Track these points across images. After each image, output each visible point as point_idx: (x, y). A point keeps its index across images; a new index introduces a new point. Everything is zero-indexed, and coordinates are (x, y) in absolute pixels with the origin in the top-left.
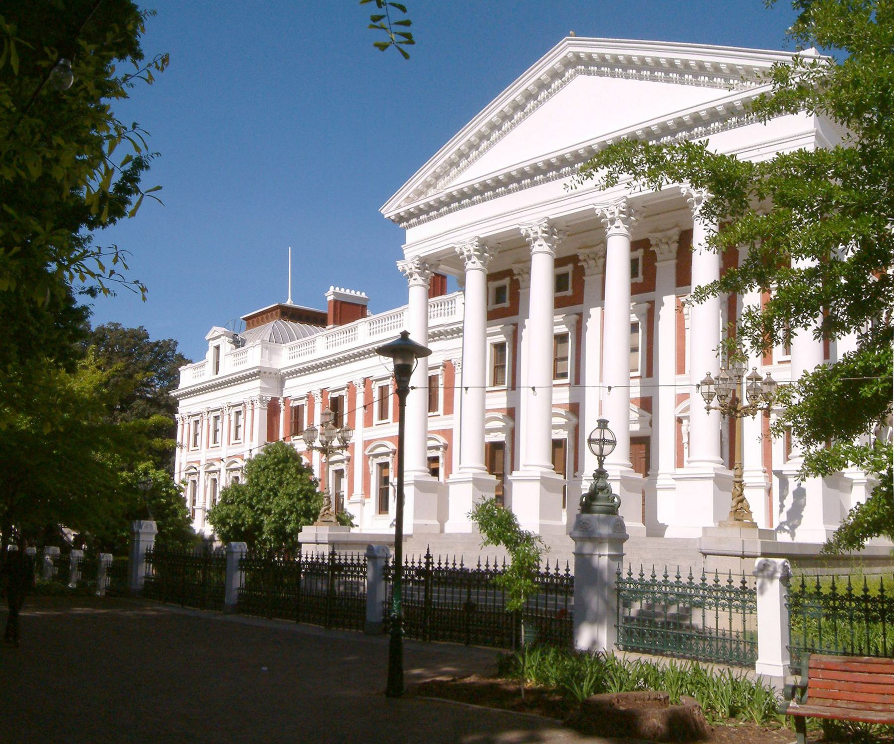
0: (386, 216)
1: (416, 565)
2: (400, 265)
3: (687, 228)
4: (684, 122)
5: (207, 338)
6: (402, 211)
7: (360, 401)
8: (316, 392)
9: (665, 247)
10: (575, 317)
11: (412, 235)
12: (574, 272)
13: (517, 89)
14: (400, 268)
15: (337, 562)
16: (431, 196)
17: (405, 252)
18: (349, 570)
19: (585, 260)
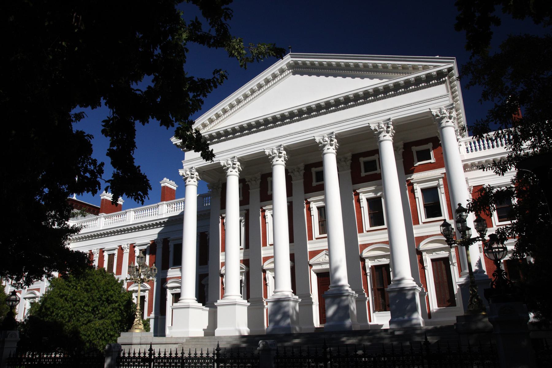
0: (174, 143)
1: (142, 355)
2: (181, 172)
9: (253, 182)
10: (245, 211)
13: (276, 67)
14: (181, 174)
17: (184, 165)
18: (131, 362)
19: (292, 172)
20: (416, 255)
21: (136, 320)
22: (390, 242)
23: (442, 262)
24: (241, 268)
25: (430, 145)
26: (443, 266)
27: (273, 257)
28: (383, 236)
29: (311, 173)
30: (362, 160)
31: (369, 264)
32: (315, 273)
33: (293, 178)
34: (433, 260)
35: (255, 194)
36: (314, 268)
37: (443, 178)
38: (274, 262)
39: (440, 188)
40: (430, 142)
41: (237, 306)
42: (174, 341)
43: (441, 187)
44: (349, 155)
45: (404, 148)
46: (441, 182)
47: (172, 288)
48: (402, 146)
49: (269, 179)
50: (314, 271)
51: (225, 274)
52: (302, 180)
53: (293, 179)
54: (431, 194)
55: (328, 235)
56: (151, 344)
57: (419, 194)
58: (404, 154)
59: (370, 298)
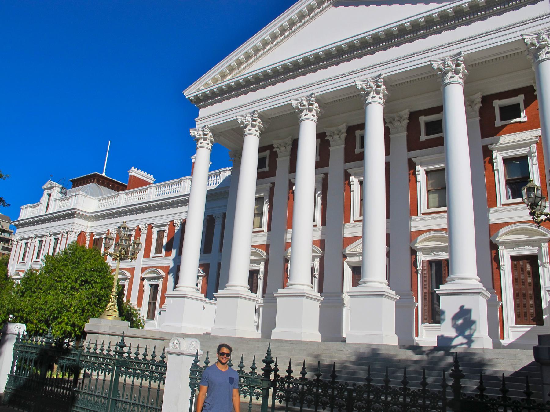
0: (187, 97)
2: (193, 132)
3: (295, 138)
4: (462, 10)
5: (44, 187)
6: (199, 94)
7: (143, 239)
8: (143, 226)
10: (322, 175)
11: (202, 112)
12: (270, 156)
15: (126, 355)
16: (230, 80)
17: (197, 123)
19: (330, 136)
20: (489, 251)
21: (110, 304)
22: (449, 230)
23: (527, 262)
24: (314, 252)
25: (520, 99)
26: (528, 268)
27: (362, 237)
28: (441, 222)
29: (355, 137)
30: (423, 119)
31: (421, 257)
32: (350, 266)
33: (392, 131)
34: (514, 259)
35: (337, 151)
36: (349, 259)
37: (537, 143)
38: (363, 243)
39: (531, 157)
40: (520, 94)
41: (186, 299)
42: (158, 336)
43: (533, 155)
44: (478, 97)
45: (482, 102)
46: (534, 148)
47: (509, 245)
48: (480, 100)
49: (358, 133)
50: (348, 263)
51: (290, 258)
52: (343, 146)
53: (278, 156)
54: (517, 166)
55: (364, 218)
56: (123, 337)
57: (499, 165)
58: (482, 111)
59: (420, 304)
